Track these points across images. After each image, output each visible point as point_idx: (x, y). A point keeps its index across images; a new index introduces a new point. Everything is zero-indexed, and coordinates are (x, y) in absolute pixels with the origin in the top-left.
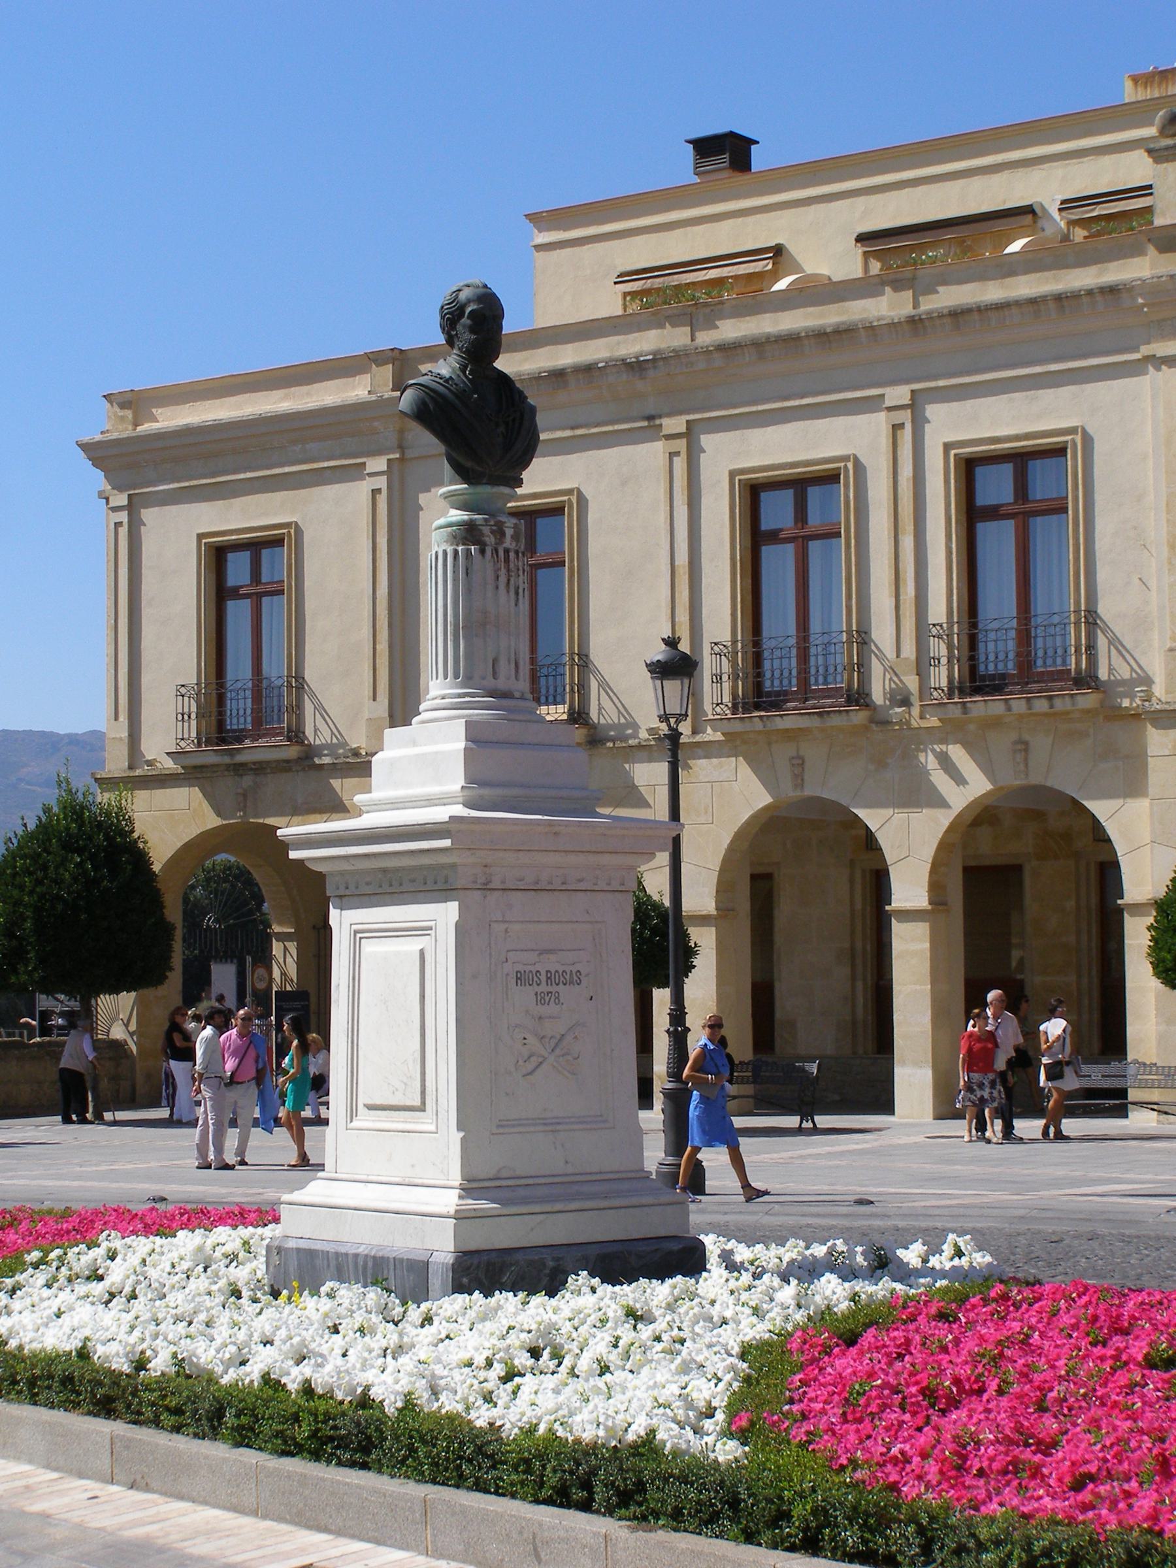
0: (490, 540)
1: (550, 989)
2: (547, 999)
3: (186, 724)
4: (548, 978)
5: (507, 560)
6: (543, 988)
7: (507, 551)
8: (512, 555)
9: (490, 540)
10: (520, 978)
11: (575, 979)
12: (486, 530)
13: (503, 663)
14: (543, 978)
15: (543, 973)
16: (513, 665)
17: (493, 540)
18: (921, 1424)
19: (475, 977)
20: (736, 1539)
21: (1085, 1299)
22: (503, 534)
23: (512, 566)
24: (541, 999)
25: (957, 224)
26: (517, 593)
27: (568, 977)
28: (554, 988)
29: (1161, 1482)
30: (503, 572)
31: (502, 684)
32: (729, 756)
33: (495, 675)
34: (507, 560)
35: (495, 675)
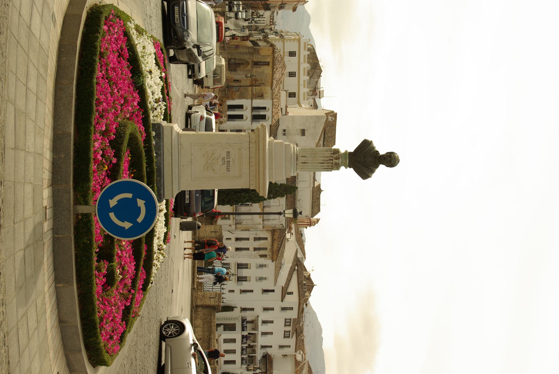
0: (335, 156)
5: (330, 160)
6: (226, 160)
7: (332, 160)
8: (331, 161)
9: (335, 156)
10: (228, 152)
11: (228, 170)
12: (337, 155)
13: (304, 158)
18: (211, 277)
19: (229, 139)
20: (144, 295)
21: (246, 24)
25: (288, 285)
26: (322, 163)
30: (327, 159)
31: (299, 158)
33: (302, 156)
34: (330, 160)
35: (302, 156)
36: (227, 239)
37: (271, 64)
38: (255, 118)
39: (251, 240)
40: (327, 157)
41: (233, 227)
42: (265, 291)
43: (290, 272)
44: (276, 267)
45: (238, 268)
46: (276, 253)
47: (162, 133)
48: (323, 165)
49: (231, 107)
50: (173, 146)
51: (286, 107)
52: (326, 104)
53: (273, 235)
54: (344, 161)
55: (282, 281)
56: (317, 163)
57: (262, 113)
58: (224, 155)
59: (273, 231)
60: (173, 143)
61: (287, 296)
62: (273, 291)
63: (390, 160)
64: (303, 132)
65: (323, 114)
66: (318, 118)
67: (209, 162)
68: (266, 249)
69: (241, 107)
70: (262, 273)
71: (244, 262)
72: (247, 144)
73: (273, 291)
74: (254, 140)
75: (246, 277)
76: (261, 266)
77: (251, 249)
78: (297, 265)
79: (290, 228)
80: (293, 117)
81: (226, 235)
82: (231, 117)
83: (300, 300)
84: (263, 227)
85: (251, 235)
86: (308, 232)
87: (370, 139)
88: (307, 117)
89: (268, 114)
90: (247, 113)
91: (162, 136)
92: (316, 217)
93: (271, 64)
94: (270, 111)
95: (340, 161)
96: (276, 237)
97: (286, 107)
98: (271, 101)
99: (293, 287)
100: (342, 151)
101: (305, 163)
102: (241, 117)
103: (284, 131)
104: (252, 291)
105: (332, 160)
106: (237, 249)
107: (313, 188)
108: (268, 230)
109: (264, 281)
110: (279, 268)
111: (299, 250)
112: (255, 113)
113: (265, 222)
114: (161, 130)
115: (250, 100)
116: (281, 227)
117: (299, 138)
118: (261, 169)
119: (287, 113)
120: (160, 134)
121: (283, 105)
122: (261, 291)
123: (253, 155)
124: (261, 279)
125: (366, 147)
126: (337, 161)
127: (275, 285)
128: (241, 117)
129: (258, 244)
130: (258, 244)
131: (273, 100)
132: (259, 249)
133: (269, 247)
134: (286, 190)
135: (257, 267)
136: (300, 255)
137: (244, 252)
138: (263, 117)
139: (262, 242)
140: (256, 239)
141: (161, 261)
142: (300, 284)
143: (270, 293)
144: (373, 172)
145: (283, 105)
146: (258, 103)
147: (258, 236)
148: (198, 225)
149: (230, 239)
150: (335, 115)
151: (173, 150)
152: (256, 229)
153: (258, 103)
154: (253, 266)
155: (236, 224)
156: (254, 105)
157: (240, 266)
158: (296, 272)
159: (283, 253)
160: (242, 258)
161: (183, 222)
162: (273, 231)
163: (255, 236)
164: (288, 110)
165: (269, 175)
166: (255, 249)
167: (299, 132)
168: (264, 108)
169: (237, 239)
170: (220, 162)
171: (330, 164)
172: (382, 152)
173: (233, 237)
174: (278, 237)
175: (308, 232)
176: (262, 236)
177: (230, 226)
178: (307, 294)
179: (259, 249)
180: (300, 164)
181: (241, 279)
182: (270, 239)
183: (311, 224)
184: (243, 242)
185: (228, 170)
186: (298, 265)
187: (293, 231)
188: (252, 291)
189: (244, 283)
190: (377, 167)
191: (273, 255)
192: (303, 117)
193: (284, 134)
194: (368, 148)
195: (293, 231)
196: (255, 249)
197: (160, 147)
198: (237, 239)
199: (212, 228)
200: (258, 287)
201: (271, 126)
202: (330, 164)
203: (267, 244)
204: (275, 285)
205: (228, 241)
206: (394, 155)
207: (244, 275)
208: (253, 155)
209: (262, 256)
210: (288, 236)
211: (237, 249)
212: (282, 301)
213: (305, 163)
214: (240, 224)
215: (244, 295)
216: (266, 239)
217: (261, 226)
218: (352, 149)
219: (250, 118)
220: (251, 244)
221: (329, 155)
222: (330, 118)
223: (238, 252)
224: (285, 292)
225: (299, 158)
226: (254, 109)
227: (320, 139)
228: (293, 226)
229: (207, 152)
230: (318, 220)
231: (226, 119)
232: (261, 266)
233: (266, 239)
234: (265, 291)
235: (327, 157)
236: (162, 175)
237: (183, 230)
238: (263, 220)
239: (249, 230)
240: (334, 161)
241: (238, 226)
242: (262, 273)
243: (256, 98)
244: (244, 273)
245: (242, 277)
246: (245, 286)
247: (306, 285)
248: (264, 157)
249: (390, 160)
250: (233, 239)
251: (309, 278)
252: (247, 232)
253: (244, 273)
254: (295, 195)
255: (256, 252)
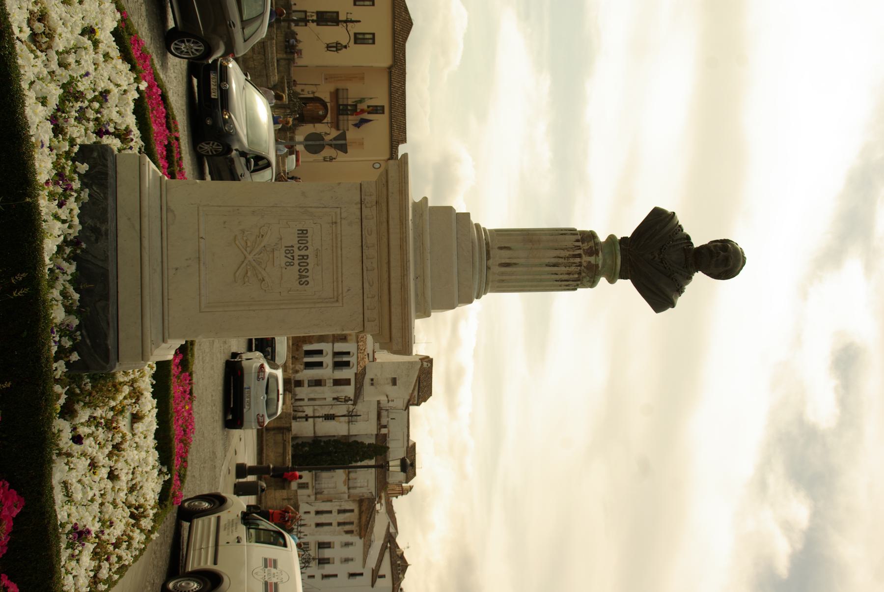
1: (296, 258)
2: (289, 255)
3: (340, 291)
4: (303, 256)
5: (575, 256)
6: (297, 253)
7: (580, 256)
8: (577, 260)
9: (586, 246)
10: (303, 233)
11: (303, 280)
12: (592, 244)
13: (505, 253)
14: (303, 253)
15: (306, 253)
16: (508, 261)
17: (586, 248)
22: (591, 255)
23: (572, 260)
24: (289, 250)
26: (554, 265)
27: (304, 273)
28: (296, 262)
29: (316, 478)
30: (567, 253)
32: (690, 278)
33: (501, 248)
34: (575, 256)
35: (501, 248)
36: (305, 513)
37: (387, 110)
38: (338, 365)
39: (335, 513)
40: (566, 249)
41: (313, 497)
42: (352, 575)
43: (381, 550)
44: (364, 545)
45: (319, 548)
46: (364, 528)
47: (110, 172)
48: (555, 269)
49: (309, 353)
50: (146, 210)
51: (374, 352)
52: (420, 349)
53: (360, 506)
54: (609, 262)
55: (372, 562)
56: (541, 265)
57: (345, 359)
58: (292, 239)
59: (361, 502)
60: (145, 203)
61: (378, 580)
62: (361, 574)
63: (723, 260)
64: (394, 382)
65: (417, 359)
66: (412, 364)
67: (250, 257)
68: (352, 523)
69: (320, 352)
70: (348, 552)
71: (326, 540)
72: (355, 209)
73: (361, 574)
74: (374, 198)
75: (329, 559)
76: (347, 544)
77: (335, 524)
78: (389, 541)
79: (380, 498)
80: (382, 365)
81: (303, 507)
82: (309, 365)
83: (393, 584)
84: (349, 497)
85: (334, 506)
86: (399, 503)
87: (668, 207)
88: (399, 363)
89: (353, 360)
90: (328, 360)
91: (111, 180)
92: (411, 483)
93: (387, 110)
94: (355, 356)
95: (600, 260)
96: (364, 508)
97: (374, 352)
98: (356, 345)
99: (386, 568)
100: (602, 238)
101: (508, 265)
102: (320, 364)
103: (372, 380)
104: (336, 576)
105: (580, 256)
106: (318, 525)
107: (408, 447)
108: (354, 501)
109: (350, 563)
110: (368, 546)
111: (391, 524)
112: (337, 360)
113: (352, 491)
114: (110, 164)
115: (331, 344)
116: (370, 496)
117: (389, 389)
118: (395, 274)
119: (374, 359)
120: (106, 174)
121: (370, 352)
122: (347, 575)
123: (371, 239)
124: (347, 560)
125: (659, 226)
126: (592, 259)
127: (364, 567)
128: (320, 364)
129: (342, 518)
130: (342, 518)
131: (358, 342)
132: (344, 524)
133: (356, 521)
134: (377, 450)
135: (342, 546)
136: (392, 530)
137: (326, 528)
138: (347, 364)
139: (348, 514)
140: (340, 512)
141: (135, 544)
142: (393, 564)
143: (358, 578)
144: (680, 291)
145: (369, 350)
146: (340, 347)
147: (343, 508)
148: (262, 486)
149: (309, 512)
150: (430, 361)
151: (145, 221)
152: (340, 499)
153: (340, 347)
154: (337, 545)
155: (316, 494)
156: (336, 350)
157: (322, 545)
158: (388, 550)
159: (372, 527)
160: (324, 536)
161: (239, 483)
162: (361, 502)
163: (338, 508)
164: (376, 356)
165: (417, 295)
166: (339, 524)
167: (389, 381)
168: (348, 353)
169: (318, 513)
170: (281, 258)
171: (573, 269)
172: (700, 237)
173: (312, 510)
174: (366, 509)
175: (399, 503)
176: (348, 508)
177: (309, 496)
178: (401, 576)
179: (344, 524)
180: (496, 269)
181: (323, 561)
182: (356, 511)
183: (403, 492)
184: (325, 515)
185: (303, 280)
186: (390, 539)
187: (383, 501)
188: (336, 576)
189: (326, 566)
190: (689, 278)
191: (360, 530)
192: (393, 363)
193: (372, 384)
194: (669, 226)
195: (383, 501)
196: (339, 524)
197: (105, 211)
198: (318, 513)
199: (284, 493)
200: (342, 570)
201: (356, 374)
202: (573, 269)
203: (353, 517)
204: (364, 567)
205: (307, 516)
206: (733, 245)
207: (326, 556)
208: (371, 239)
209: (347, 532)
210: (378, 506)
211: (318, 525)
212: (373, 586)
213: (508, 265)
214: (321, 493)
215: (326, 581)
216: (352, 511)
217: (346, 496)
218: (626, 230)
219: (331, 365)
220: (334, 518)
221: (569, 244)
222: (425, 364)
223: (320, 529)
224: (376, 575)
225: (491, 253)
226: (336, 354)
227: (414, 389)
228: (383, 495)
229: (243, 231)
230: (411, 488)
231: (302, 367)
232: (347, 544)
233: (352, 511)
234: (352, 575)
235: (566, 249)
236: (112, 292)
237: (238, 495)
238: (349, 489)
239: (331, 501)
240: (586, 259)
241: (319, 496)
242: (348, 552)
243: (338, 341)
244: (327, 553)
245: (324, 559)
246: (328, 569)
247: (400, 566)
248: (403, 240)
249: (723, 260)
250: (313, 514)
251: (402, 557)
252: (329, 503)
253: (327, 553)
254: (386, 456)
255: (340, 527)
